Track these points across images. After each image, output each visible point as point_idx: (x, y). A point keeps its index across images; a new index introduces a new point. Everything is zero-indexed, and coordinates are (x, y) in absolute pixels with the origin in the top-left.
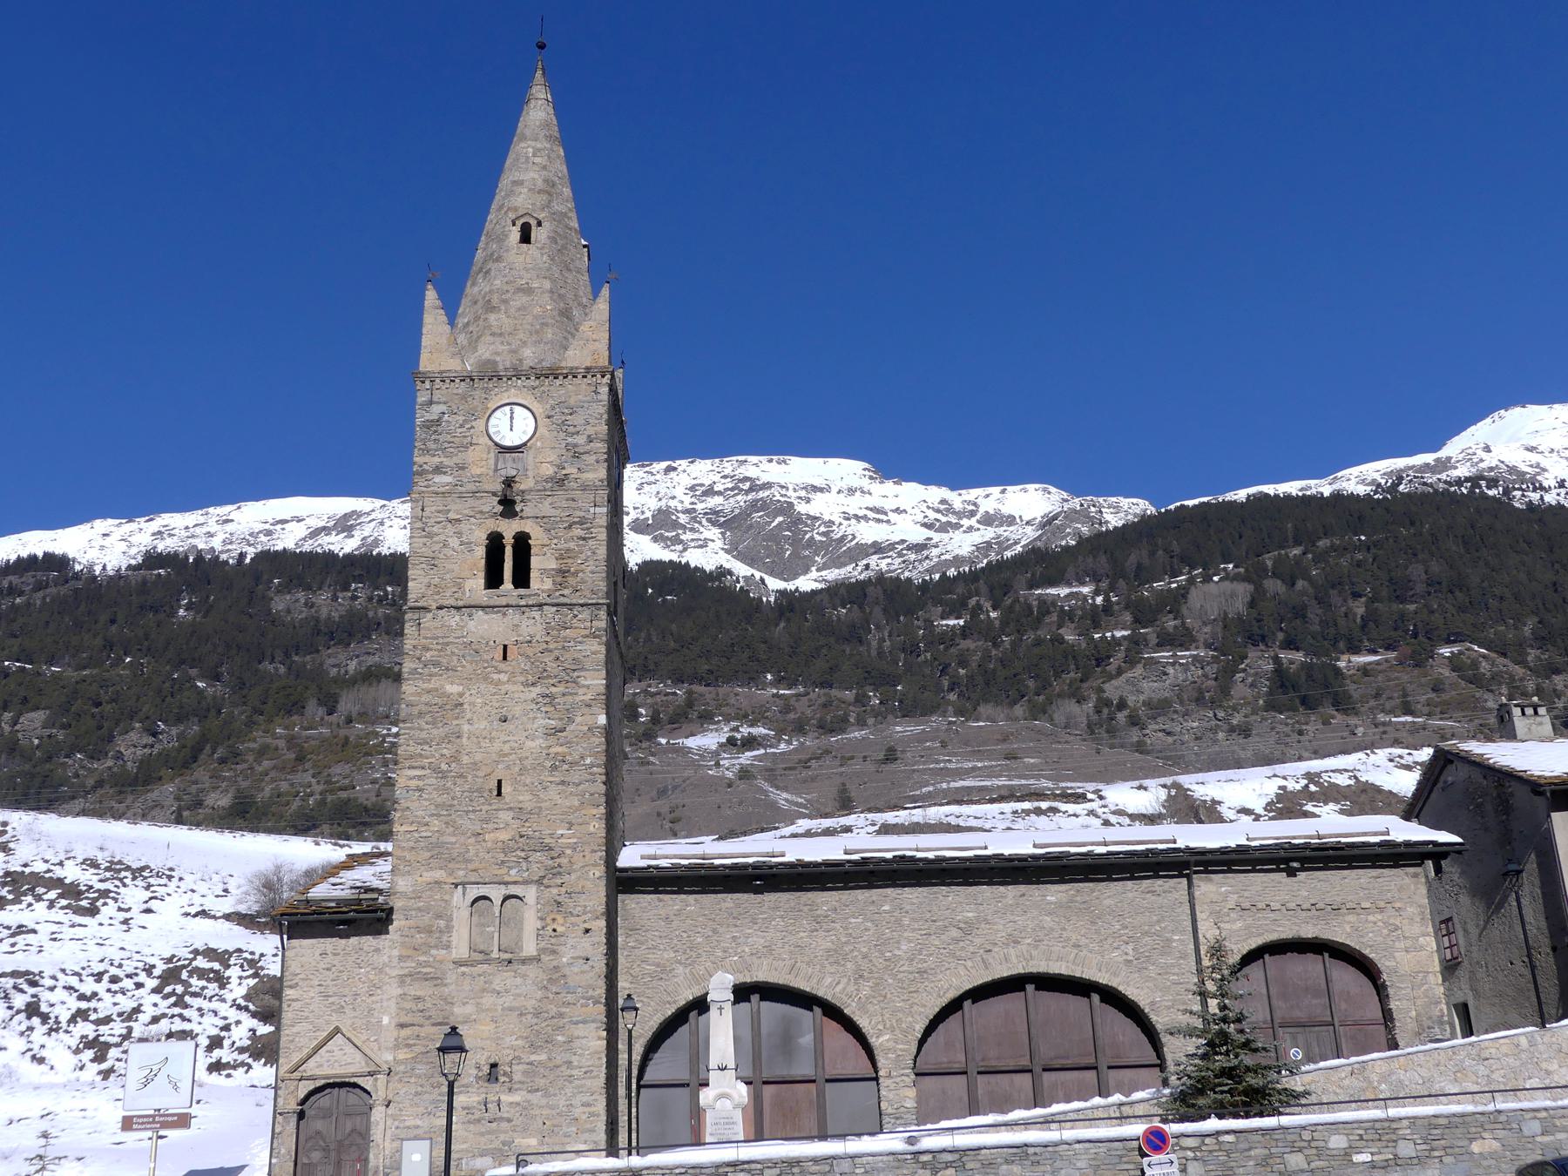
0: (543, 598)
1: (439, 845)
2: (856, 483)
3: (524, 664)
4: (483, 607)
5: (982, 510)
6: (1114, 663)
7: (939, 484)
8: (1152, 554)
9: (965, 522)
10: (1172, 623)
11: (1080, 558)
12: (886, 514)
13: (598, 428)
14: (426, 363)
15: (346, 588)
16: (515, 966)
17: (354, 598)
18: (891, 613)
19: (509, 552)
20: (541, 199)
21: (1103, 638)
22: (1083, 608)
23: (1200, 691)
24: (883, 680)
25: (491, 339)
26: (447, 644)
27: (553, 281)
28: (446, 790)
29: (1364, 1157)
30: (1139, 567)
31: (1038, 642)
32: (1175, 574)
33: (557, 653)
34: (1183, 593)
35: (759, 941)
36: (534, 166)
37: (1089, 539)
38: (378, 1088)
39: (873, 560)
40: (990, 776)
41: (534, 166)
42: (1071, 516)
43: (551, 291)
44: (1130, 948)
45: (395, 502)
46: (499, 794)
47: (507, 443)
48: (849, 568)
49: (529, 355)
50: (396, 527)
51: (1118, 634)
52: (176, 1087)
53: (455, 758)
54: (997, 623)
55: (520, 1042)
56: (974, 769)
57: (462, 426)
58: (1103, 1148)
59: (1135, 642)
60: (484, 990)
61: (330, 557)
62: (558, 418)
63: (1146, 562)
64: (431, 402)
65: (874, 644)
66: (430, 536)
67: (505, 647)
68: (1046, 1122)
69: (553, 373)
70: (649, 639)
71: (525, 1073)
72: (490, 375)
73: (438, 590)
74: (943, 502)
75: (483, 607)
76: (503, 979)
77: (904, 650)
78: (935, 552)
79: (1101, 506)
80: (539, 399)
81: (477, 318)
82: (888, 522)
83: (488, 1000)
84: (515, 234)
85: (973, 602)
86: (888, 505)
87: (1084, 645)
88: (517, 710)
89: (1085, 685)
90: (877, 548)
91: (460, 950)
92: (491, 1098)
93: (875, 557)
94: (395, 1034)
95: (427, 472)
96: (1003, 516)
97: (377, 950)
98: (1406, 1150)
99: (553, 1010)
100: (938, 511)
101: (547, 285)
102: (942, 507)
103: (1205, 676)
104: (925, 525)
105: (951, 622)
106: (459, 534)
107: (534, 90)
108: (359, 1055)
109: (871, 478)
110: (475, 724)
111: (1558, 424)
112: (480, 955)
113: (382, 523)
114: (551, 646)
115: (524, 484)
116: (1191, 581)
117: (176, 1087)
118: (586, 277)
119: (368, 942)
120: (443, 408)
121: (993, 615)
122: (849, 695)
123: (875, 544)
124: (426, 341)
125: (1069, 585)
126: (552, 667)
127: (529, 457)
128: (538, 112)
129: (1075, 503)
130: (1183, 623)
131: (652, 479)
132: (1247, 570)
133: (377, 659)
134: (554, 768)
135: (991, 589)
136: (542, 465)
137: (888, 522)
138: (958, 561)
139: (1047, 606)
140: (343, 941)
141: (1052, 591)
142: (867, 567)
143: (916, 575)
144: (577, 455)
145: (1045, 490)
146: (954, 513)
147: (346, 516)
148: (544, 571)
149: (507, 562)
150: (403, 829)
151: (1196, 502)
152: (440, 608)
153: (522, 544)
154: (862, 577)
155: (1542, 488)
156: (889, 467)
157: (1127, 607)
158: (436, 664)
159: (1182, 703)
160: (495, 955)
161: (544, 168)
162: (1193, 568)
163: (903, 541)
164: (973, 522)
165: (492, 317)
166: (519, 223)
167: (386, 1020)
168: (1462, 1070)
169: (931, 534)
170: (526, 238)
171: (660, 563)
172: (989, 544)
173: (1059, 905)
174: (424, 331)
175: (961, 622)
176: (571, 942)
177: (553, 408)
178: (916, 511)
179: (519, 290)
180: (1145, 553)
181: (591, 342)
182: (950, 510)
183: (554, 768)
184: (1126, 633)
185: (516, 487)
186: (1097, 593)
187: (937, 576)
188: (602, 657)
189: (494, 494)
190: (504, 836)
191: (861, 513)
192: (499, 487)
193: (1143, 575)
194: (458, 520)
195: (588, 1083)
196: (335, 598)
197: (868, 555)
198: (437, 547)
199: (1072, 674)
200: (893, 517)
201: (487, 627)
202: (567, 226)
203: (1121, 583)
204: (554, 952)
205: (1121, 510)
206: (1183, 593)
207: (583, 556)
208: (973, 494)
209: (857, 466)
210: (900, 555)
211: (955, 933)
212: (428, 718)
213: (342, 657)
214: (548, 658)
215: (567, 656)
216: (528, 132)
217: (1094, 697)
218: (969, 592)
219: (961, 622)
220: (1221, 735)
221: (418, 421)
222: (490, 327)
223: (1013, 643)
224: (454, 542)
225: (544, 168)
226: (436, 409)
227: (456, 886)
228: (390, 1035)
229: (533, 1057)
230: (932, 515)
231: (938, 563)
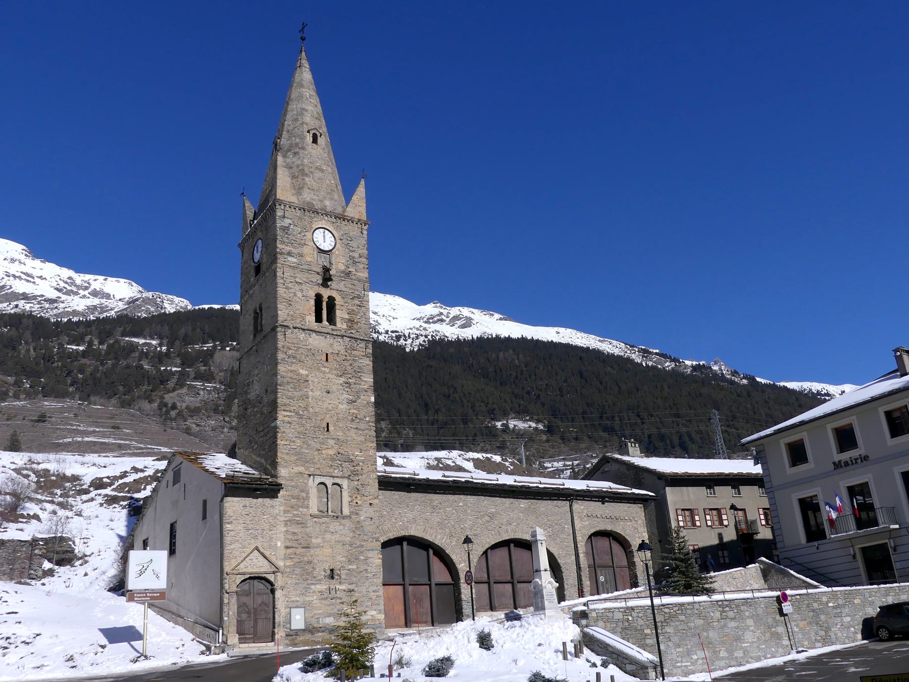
0: (343, 333)
1: (300, 453)
2: (17, 257)
5: (92, 288)
6: (171, 384)
7: (69, 268)
8: (194, 330)
9: (82, 292)
12: (33, 278)
16: (339, 520)
18: (36, 336)
23: (218, 406)
24: (34, 374)
28: (303, 425)
29: (831, 605)
30: (186, 335)
33: (351, 362)
34: (210, 353)
35: (410, 516)
36: (306, 104)
38: (279, 581)
39: (21, 303)
40: (104, 437)
42: (146, 301)
44: (550, 530)
46: (328, 430)
47: (322, 248)
48: (5, 305)
51: (174, 369)
52: (158, 577)
53: (306, 409)
54: (103, 352)
55: (344, 559)
56: (94, 432)
58: (767, 600)
59: (183, 375)
60: (325, 531)
64: (284, 217)
65: (23, 351)
68: (616, 599)
71: (347, 574)
73: (293, 318)
74: (70, 278)
76: (335, 526)
78: (62, 305)
80: (338, 228)
82: (34, 283)
83: (328, 536)
84: (309, 139)
85: (88, 338)
86: (36, 273)
88: (334, 388)
89: (154, 394)
90: (25, 297)
91: (314, 510)
92: (332, 587)
93: (23, 301)
94: (284, 552)
96: (104, 293)
97: (272, 506)
98: (840, 602)
99: (358, 543)
100: (66, 283)
102: (69, 281)
103: (219, 398)
104: (57, 289)
105: (74, 347)
106: (302, 290)
108: (266, 562)
109: (26, 255)
110: (314, 392)
111: (387, 303)
112: (323, 513)
114: (348, 358)
116: (215, 347)
117: (158, 577)
119: (268, 501)
122: (11, 379)
123: (24, 294)
125: (145, 338)
129: (150, 295)
134: (353, 420)
135: (100, 333)
137: (34, 283)
138: (75, 313)
139: (133, 347)
140: (255, 500)
141: (136, 340)
142: (17, 306)
143: (50, 314)
144: (355, 263)
146: (76, 286)
150: (283, 443)
152: (295, 328)
154: (12, 312)
155: (378, 332)
156: (38, 251)
158: (294, 357)
159: (206, 410)
160: (330, 513)
163: (42, 296)
164: (86, 293)
166: (312, 132)
167: (279, 544)
168: (729, 582)
169: (60, 294)
170: (315, 140)
172: (95, 307)
173: (525, 509)
175: (81, 348)
176: (364, 509)
179: (317, 168)
180: (190, 328)
181: (358, 207)
182: (73, 283)
183: (353, 420)
186: (161, 345)
187: (66, 320)
188: (371, 368)
190: (331, 452)
191: (17, 274)
193: (187, 340)
195: (375, 580)
197: (18, 299)
199: (145, 387)
200: (37, 280)
201: (316, 342)
204: (357, 514)
205: (173, 304)
206: (210, 353)
208: (87, 277)
209: (19, 247)
210: (39, 303)
211: (487, 518)
212: (292, 385)
214: (347, 364)
215: (356, 364)
217: (158, 401)
219: (81, 348)
220: (226, 430)
223: (113, 365)
224: (299, 294)
226: (287, 222)
227: (310, 475)
228: (282, 552)
229: (350, 567)
230: (62, 284)
231: (63, 312)
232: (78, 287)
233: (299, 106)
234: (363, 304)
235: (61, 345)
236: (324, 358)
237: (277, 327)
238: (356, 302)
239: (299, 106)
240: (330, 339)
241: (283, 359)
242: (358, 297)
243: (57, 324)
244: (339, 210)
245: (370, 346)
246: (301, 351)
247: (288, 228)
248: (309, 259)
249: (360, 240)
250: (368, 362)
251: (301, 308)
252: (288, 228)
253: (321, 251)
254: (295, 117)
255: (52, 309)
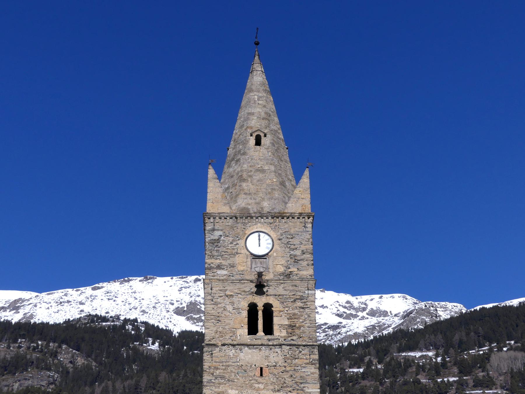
0: (282, 341)
3: (272, 379)
4: (248, 345)
8: (468, 334)
9: (360, 314)
10: (481, 374)
11: (427, 336)
13: (307, 247)
14: (210, 208)
15: (15, 341)
17: (20, 347)
19: (260, 314)
20: (264, 123)
21: (443, 382)
22: (430, 364)
25: (245, 196)
26: (228, 366)
27: (275, 166)
31: (406, 383)
32: (481, 346)
33: (291, 373)
34: (487, 357)
36: (257, 106)
37: (431, 326)
41: (257, 106)
42: (420, 312)
43: (275, 172)
45: (44, 294)
49: (267, 206)
50: (43, 308)
51: (451, 379)
54: (382, 371)
57: (231, 243)
61: (8, 323)
62: (285, 240)
63: (465, 339)
64: (213, 230)
66: (216, 304)
67: (261, 369)
69: (281, 216)
70: (185, 375)
72: (246, 216)
73: (222, 334)
75: (248, 345)
77: (329, 385)
78: (344, 330)
79: (436, 307)
80: (274, 229)
81: (234, 185)
84: (252, 141)
85: (367, 359)
87: (432, 385)
95: (213, 268)
96: (381, 311)
101: (273, 168)
102: (347, 305)
104: (338, 315)
105: (355, 370)
106: (232, 303)
107: (255, 66)
113: (36, 306)
114: (288, 369)
115: (267, 277)
116: (491, 350)
118: (290, 165)
120: (220, 233)
121: (379, 366)
124: (209, 196)
125: (421, 351)
126: (289, 381)
127: (270, 262)
128: (258, 78)
129: (422, 305)
130: (488, 374)
131: (187, 285)
132: (522, 345)
133: (30, 382)
135: (378, 352)
136: (277, 266)
138: (356, 335)
139: (409, 362)
141: (412, 354)
143: (334, 342)
144: (296, 261)
145: (404, 297)
146: (354, 309)
147: (16, 301)
148: (281, 326)
149: (259, 320)
151: (490, 305)
152: (224, 345)
153: (268, 310)
157: (455, 364)
158: (222, 377)
161: (264, 106)
162: (491, 343)
163: (326, 324)
164: (364, 314)
165: (244, 185)
166: (254, 135)
169: (341, 320)
170: (258, 142)
171: (191, 332)
172: (374, 327)
174: (209, 191)
175: (361, 370)
177: (282, 235)
178: (333, 307)
179: (258, 170)
180: (464, 334)
181: (301, 199)
182: (352, 307)
184: (455, 379)
185: (263, 277)
186: (437, 356)
187: (346, 344)
188: (317, 376)
189: (252, 281)
192: (254, 277)
193: (463, 346)
194: (231, 296)
196: (9, 347)
198: (220, 310)
201: (250, 357)
202: (278, 138)
203: (452, 351)
205: (447, 310)
206: (487, 357)
207: (303, 318)
210: (324, 331)
213: (10, 381)
214: (286, 376)
215: (298, 375)
216: (254, 88)
218: (365, 353)
221: (207, 240)
222: (243, 190)
223: (392, 383)
224: (230, 308)
225: (264, 106)
226: (217, 234)
230: (342, 310)
231: (345, 337)
232: (357, 310)
233: (246, 111)
234: (306, 304)
235: (343, 370)
236: (258, 373)
237: (203, 347)
238: (299, 304)
239: (246, 111)
240: (265, 351)
241: (210, 381)
242: (301, 298)
243: (340, 349)
244: (279, 208)
245: (316, 351)
246: (229, 369)
247: (218, 240)
248: (242, 268)
249: (303, 235)
250: (313, 370)
251: (232, 322)
252: (218, 240)
253: (256, 257)
254: (242, 124)
255: (335, 335)
